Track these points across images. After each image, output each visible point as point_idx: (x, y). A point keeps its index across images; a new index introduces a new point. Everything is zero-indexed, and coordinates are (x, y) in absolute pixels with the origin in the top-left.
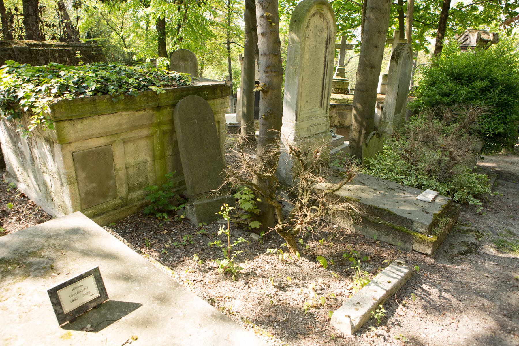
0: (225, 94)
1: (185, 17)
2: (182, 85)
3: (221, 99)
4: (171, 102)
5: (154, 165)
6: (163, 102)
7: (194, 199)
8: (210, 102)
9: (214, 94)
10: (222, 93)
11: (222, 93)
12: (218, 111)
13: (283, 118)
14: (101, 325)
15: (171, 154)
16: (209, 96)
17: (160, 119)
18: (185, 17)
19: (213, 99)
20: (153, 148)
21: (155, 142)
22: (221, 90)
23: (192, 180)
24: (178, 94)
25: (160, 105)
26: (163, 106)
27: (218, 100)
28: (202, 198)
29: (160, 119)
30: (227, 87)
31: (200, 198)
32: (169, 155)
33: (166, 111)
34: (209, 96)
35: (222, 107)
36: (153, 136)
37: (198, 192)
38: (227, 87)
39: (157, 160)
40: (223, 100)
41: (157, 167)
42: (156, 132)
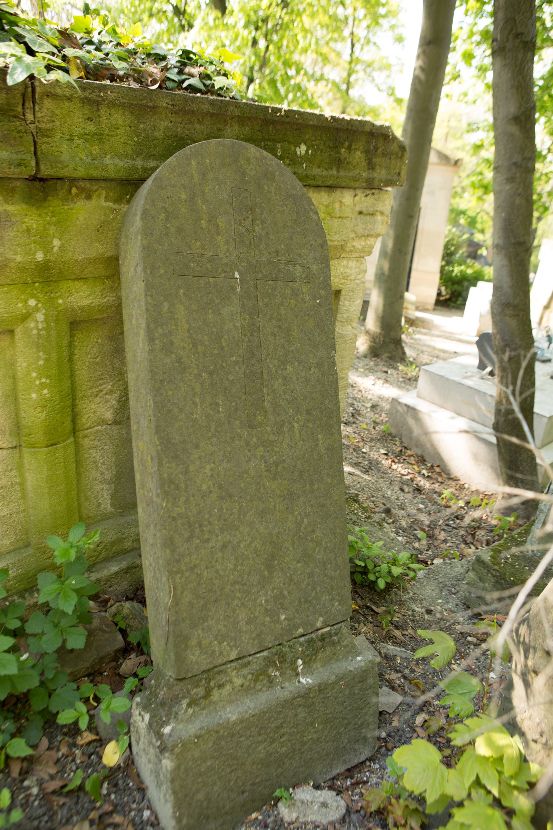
0: (380, 174)
1: (264, 63)
2: (191, 88)
3: (361, 194)
4: (114, 165)
5: (20, 467)
6: (69, 154)
7: (176, 700)
8: (320, 199)
9: (339, 163)
10: (371, 166)
11: (371, 166)
12: (342, 247)
13: (490, 297)
14: (98, 566)
15: (109, 415)
16: (316, 171)
17: (47, 248)
18: (264, 63)
19: (331, 188)
20: (14, 388)
21: (22, 364)
22: (367, 152)
23: (177, 601)
24: (162, 126)
25: (46, 171)
26: (73, 181)
27: (347, 197)
28: (216, 695)
29: (47, 248)
30: (394, 147)
31: (208, 694)
32: (103, 422)
33: (85, 212)
34: (316, 171)
35: (360, 230)
36: (11, 332)
37: (197, 660)
38: (394, 147)
39: (32, 446)
40: (370, 200)
41: (31, 479)
42: (25, 318)
